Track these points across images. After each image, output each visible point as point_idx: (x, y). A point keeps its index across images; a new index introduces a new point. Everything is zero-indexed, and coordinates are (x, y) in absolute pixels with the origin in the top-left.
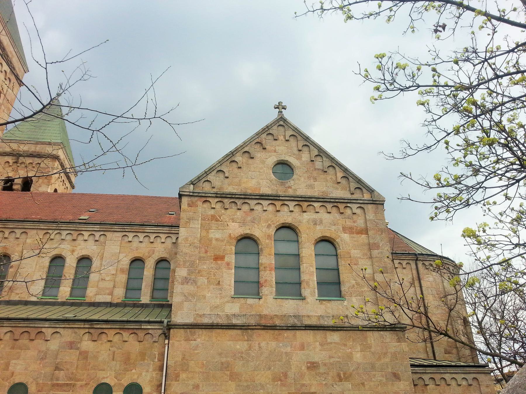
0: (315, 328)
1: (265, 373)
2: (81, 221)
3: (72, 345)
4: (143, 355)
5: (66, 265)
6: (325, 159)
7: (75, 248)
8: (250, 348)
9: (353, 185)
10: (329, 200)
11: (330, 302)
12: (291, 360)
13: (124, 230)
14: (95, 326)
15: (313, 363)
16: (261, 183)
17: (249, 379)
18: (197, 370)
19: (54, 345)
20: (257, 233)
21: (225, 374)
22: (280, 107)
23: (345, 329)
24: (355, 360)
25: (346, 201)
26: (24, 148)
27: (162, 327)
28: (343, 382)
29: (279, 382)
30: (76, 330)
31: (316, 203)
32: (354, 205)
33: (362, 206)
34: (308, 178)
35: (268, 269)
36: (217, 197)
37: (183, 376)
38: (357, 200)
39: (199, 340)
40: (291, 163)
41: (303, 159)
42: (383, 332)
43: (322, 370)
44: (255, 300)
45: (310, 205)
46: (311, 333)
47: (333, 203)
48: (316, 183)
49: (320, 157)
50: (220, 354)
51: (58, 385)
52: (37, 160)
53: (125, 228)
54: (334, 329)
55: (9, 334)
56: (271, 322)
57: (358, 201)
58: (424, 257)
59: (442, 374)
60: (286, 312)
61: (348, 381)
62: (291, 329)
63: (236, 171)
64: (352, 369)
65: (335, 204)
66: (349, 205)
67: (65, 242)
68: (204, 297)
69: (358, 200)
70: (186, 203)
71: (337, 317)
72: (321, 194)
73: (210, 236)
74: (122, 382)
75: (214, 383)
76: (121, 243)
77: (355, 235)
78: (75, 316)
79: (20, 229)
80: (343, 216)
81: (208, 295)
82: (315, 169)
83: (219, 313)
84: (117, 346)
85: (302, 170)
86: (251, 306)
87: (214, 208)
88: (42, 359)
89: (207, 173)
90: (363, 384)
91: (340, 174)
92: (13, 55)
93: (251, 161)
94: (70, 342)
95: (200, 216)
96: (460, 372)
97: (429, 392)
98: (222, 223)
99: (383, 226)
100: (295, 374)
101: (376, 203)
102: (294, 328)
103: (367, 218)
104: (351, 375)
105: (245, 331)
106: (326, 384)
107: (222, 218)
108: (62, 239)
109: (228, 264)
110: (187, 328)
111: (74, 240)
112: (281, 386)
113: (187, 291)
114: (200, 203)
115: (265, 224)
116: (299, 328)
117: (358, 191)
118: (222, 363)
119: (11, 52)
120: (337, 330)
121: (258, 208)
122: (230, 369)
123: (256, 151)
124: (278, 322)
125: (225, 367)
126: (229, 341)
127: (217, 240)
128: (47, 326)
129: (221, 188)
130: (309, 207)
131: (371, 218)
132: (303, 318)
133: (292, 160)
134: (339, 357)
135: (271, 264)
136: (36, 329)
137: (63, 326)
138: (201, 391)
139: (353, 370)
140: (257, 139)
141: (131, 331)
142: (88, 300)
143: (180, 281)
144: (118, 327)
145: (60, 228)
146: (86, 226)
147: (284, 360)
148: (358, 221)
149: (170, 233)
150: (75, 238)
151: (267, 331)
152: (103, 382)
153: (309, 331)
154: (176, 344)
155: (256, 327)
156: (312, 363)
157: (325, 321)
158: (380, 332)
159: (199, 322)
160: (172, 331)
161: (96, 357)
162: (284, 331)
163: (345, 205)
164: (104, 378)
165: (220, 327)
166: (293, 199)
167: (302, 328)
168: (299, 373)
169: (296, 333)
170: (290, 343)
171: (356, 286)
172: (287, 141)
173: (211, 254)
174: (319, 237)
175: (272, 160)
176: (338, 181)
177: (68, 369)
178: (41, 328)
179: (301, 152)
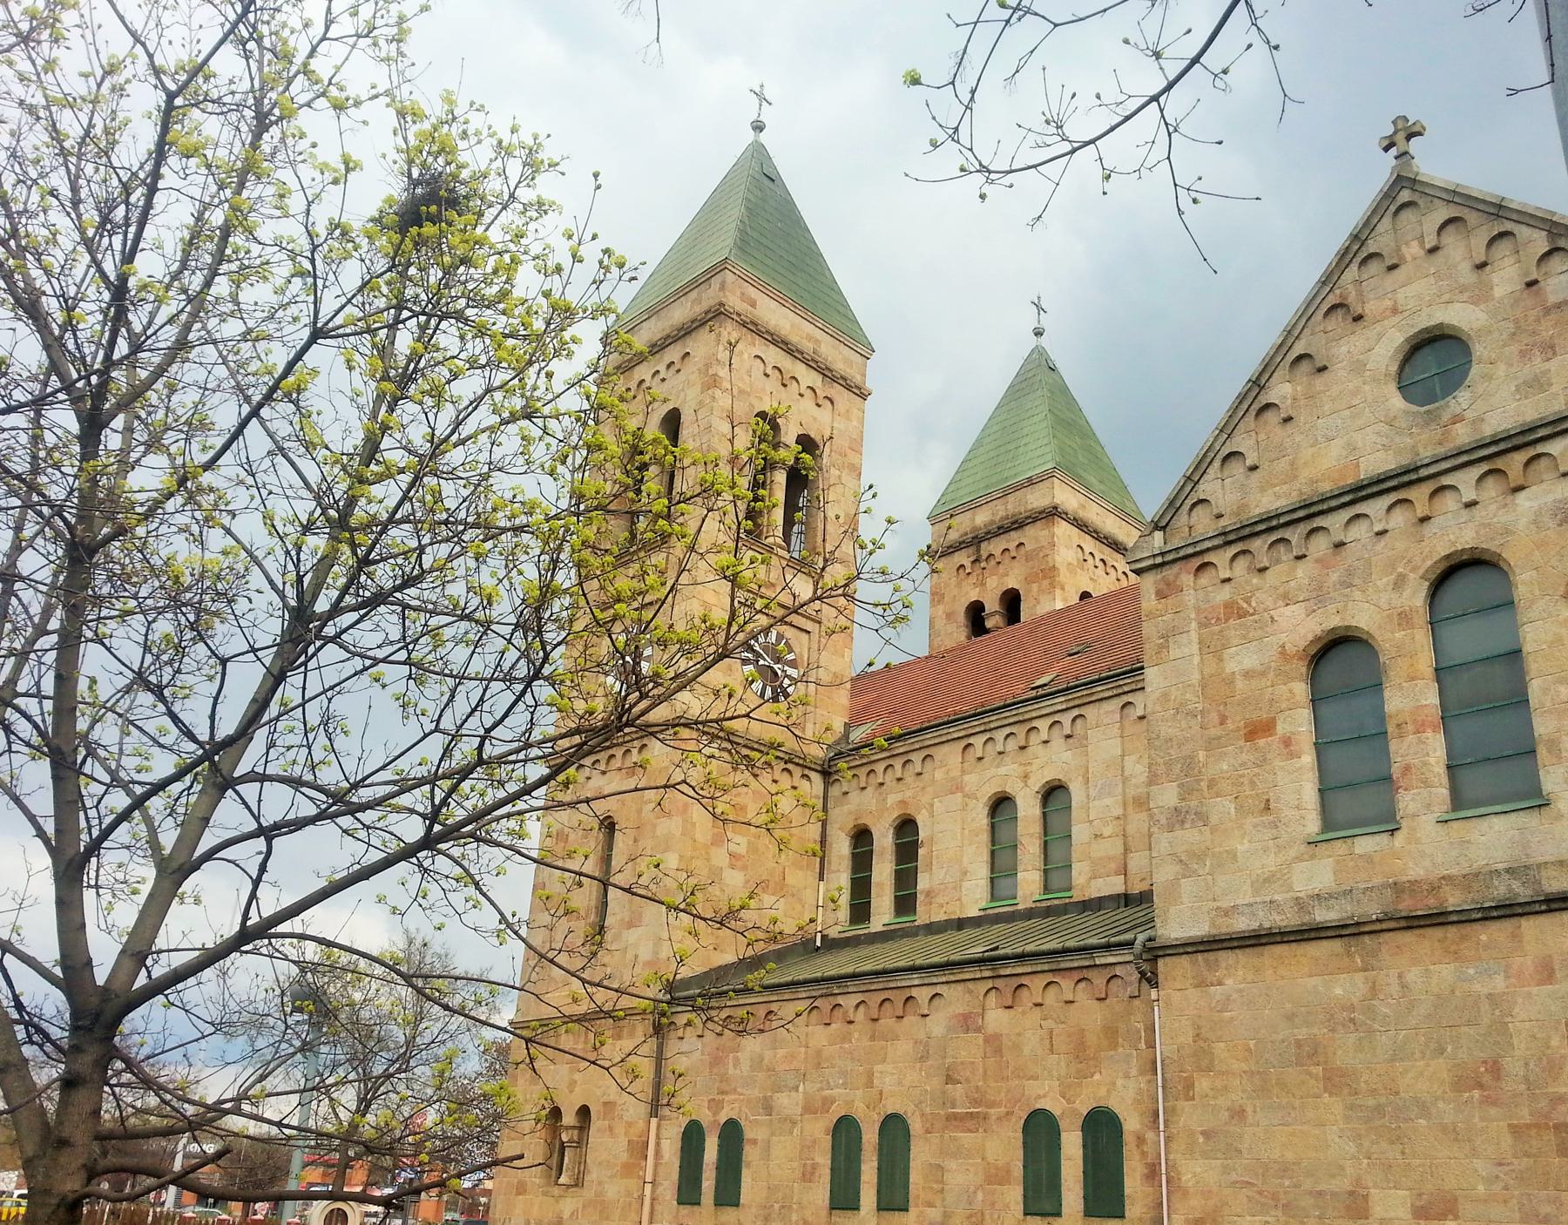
1: (1428, 1065)
2: (1041, 692)
3: (967, 1023)
4: (1111, 1034)
5: (1074, 804)
7: (1029, 768)
8: (1374, 990)
12: (1509, 1019)
13: (1120, 691)
16: (1360, 444)
17: (1379, 1086)
18: (1236, 1066)
19: (938, 1024)
20: (1363, 617)
21: (1310, 1074)
22: (1406, 132)
26: (982, 518)
27: (1131, 958)
29: (1476, 1093)
30: (970, 985)
35: (1410, 727)
37: (1203, 1084)
40: (1454, 327)
41: (1498, 292)
44: (1377, 838)
45: (1538, 456)
48: (1553, 365)
50: (1290, 1017)
51: (955, 1117)
52: (1015, 537)
53: (1121, 683)
55: (862, 1008)
56: (1432, 902)
62: (1499, 917)
63: (1279, 433)
67: (1007, 759)
68: (1234, 856)
70: (1153, 590)
73: (1227, 671)
74: (1077, 1105)
75: (1285, 1101)
76: (1122, 728)
78: (996, 948)
81: (1242, 847)
82: (1547, 311)
83: (1277, 897)
84: (1055, 1016)
85: (1496, 335)
86: (1368, 859)
87: (1229, 580)
88: (923, 1059)
89: (1192, 479)
92: (817, 342)
93: (1320, 382)
94: (963, 1015)
95: (1193, 616)
98: (1256, 617)
100: (1526, 1064)
102: (1508, 910)
105: (1353, 941)
107: (1254, 604)
108: (1000, 753)
109: (1287, 742)
110: (1196, 952)
111: (1023, 748)
112: (1481, 1103)
113: (1185, 847)
114: (1187, 579)
115: (1385, 580)
116: (1527, 909)
118: (1299, 1044)
119: (809, 338)
121: (1360, 531)
122: (1322, 1059)
124: (1454, 900)
125: (1308, 1053)
126: (1311, 976)
127: (1248, 674)
128: (916, 982)
129: (1243, 507)
130: (1535, 466)
132: (1543, 873)
133: (1460, 316)
135: (1418, 708)
137: (944, 979)
138: (1251, 1125)
140: (1331, 296)
141: (1077, 975)
142: (1077, 895)
143: (1163, 821)
144: (1046, 967)
146: (1036, 706)
147: (1486, 1021)
150: (1023, 743)
151: (1422, 931)
152: (1038, 1106)
154: (1176, 997)
155: (1384, 926)
159: (1224, 930)
160: (1161, 962)
161: (1017, 1047)
162: (1477, 926)
164: (1039, 1097)
165: (1278, 939)
166: (1465, 458)
167: (1537, 908)
173: (1236, 722)
179: (1488, 268)
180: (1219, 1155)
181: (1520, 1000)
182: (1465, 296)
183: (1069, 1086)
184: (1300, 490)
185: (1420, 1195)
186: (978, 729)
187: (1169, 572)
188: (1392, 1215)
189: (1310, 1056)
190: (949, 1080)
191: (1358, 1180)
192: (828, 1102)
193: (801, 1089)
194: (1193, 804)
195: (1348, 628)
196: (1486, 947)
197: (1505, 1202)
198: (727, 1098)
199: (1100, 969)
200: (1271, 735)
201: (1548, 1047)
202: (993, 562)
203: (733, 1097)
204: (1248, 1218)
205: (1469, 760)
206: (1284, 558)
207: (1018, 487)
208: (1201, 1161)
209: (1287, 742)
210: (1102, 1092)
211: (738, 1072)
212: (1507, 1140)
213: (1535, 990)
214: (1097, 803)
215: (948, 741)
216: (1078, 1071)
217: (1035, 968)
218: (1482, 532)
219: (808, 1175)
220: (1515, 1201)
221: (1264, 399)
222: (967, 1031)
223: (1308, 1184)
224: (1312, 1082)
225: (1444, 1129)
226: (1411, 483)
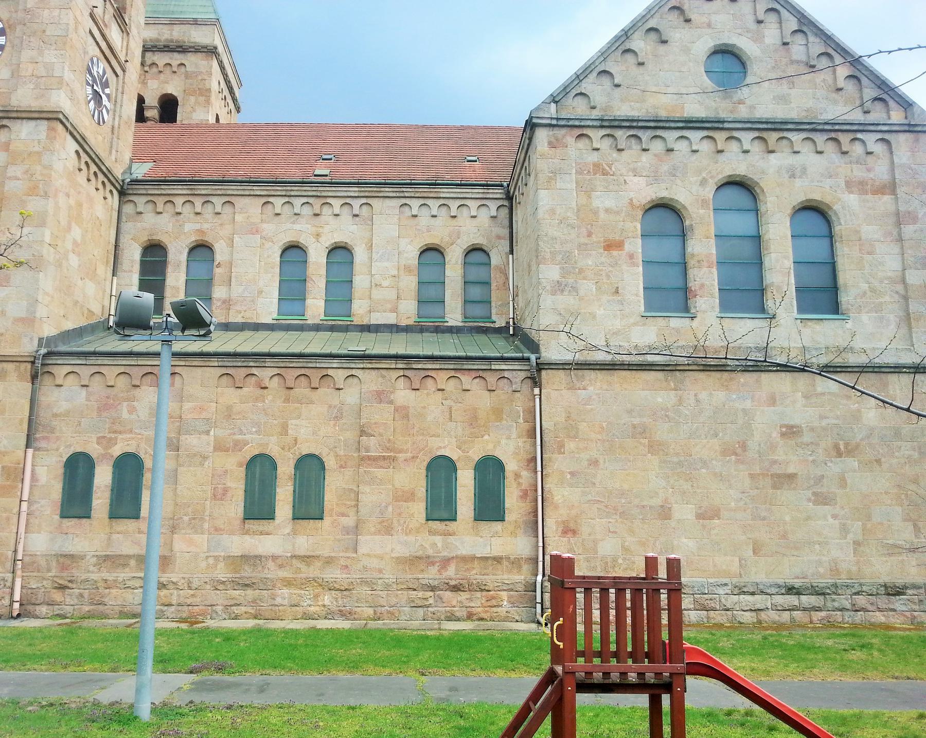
3: (380, 396)
4: (498, 413)
6: (812, 38)
8: (680, 401)
9: (870, 92)
11: (821, 322)
12: (752, 422)
13: (402, 195)
14: (414, 366)
15: (792, 427)
21: (641, 443)
23: (849, 370)
25: (855, 128)
28: (843, 458)
29: (733, 457)
30: (383, 372)
33: (887, 136)
36: (602, 127)
37: (571, 445)
39: (591, 388)
40: (741, 49)
43: (806, 438)
48: (793, 92)
50: (630, 412)
51: (369, 458)
53: (404, 190)
57: (880, 128)
63: (635, 70)
64: (859, 437)
66: (859, 136)
68: (594, 317)
72: (804, 114)
77: (869, 197)
79: (219, 197)
80: (846, 158)
81: (600, 312)
86: (678, 331)
87: (597, 149)
90: (878, 461)
93: (662, 49)
98: (615, 177)
100: (760, 445)
104: (858, 446)
105: (670, 374)
109: (631, 256)
112: (736, 462)
117: (879, 106)
118: (634, 427)
125: (639, 432)
127: (607, 211)
128: (335, 365)
131: (904, 160)
133: (745, 44)
134: (838, 418)
136: (319, 370)
137: (362, 366)
139: (862, 440)
141: (474, 374)
142: (357, 321)
144: (452, 367)
145: (288, 194)
146: (334, 189)
147: (740, 422)
149: (486, 198)
152: (439, 453)
155: (690, 368)
160: (544, 373)
165: (626, 367)
166: (749, 125)
169: (761, 377)
171: (869, 293)
175: (705, 44)
177: (381, 435)
178: (325, 369)
180: (580, 485)
181: (758, 413)
182: (749, 35)
183: (465, 442)
184: (647, 110)
185: (700, 507)
186: (279, 193)
187: (560, 132)
188: (685, 517)
189: (641, 434)
190: (363, 433)
191: (666, 500)
192: (238, 446)
193: (212, 433)
194: (571, 281)
195: (672, 199)
196: (743, 385)
197: (745, 510)
198: (120, 436)
199: (493, 372)
200: (621, 250)
201: (771, 437)
202: (155, 70)
203: (128, 436)
204: (598, 520)
205: (728, 288)
206: (634, 147)
207: (183, 22)
208: (568, 489)
209: (631, 256)
210: (490, 446)
211: (133, 416)
212: (747, 481)
213: (766, 409)
214: (378, 264)
215: (250, 195)
216: (471, 433)
217: (442, 366)
218: (750, 169)
219: (220, 495)
220: (750, 510)
221: (628, 45)
222: (380, 403)
223: (636, 502)
224: (642, 447)
225: (715, 474)
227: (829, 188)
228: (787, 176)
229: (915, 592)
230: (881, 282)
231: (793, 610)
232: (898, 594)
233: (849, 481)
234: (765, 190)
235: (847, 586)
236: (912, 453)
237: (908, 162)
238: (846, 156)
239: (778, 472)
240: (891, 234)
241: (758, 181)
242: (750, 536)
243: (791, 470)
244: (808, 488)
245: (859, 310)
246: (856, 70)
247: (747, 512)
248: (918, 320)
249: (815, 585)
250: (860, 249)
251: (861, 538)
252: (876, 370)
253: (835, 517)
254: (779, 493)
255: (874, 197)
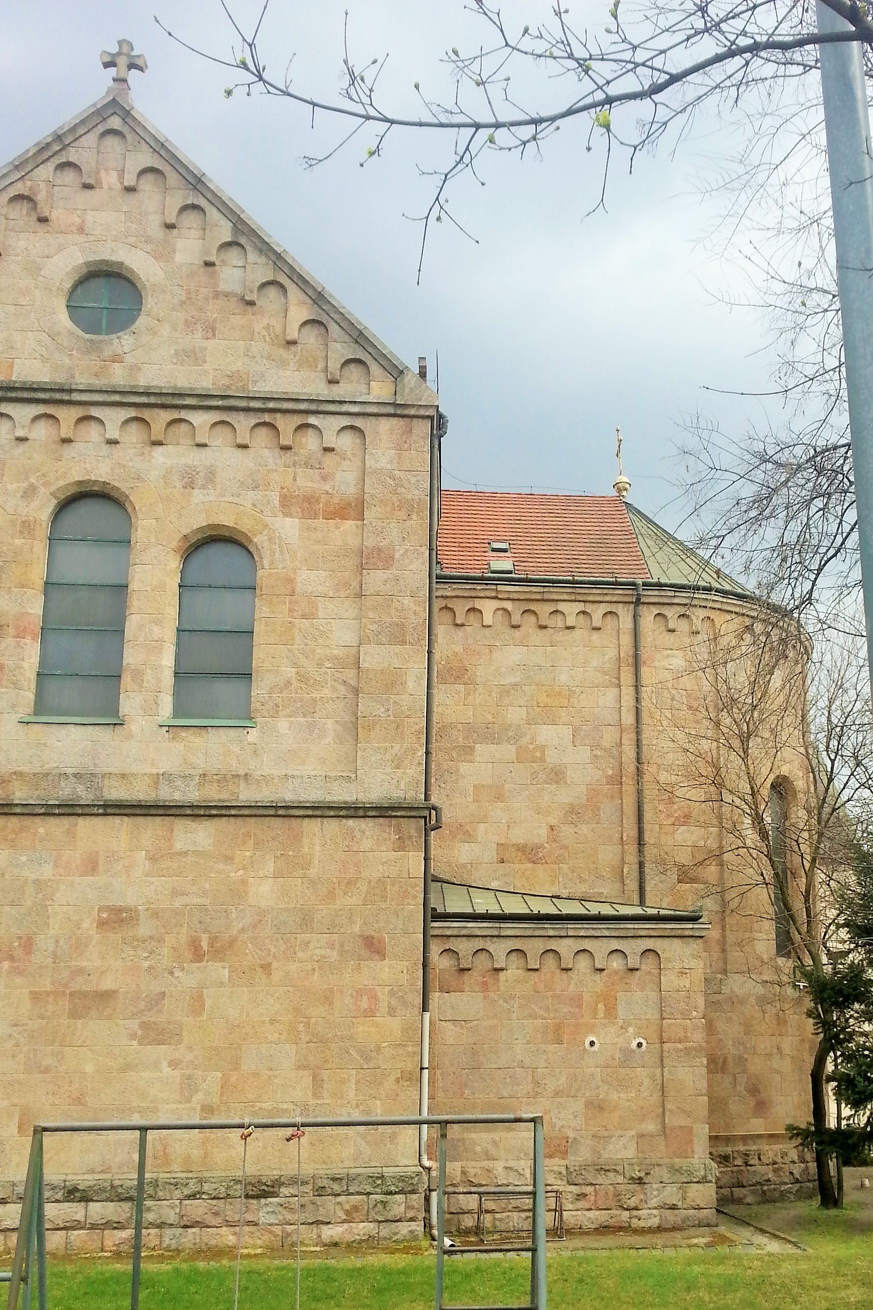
0: (138, 811)
6: (252, 256)
9: (341, 350)
10: (243, 404)
11: (203, 732)
12: (50, 902)
15: (121, 910)
23: (233, 812)
24: (252, 900)
25: (303, 406)
28: (204, 963)
31: (201, 412)
32: (331, 419)
33: (358, 422)
34: (187, 324)
35: (12, 631)
38: (341, 402)
41: (179, 258)
42: (356, 819)
43: (144, 929)
46: (122, 825)
47: (260, 414)
48: (211, 344)
49: (239, 249)
54: (196, 812)
57: (345, 408)
58: (663, 593)
59: (552, 941)
60: (56, 765)
61: (222, 960)
62: (60, 815)
64: (237, 926)
65: (267, 418)
66: (312, 420)
69: (345, 402)
71: (215, 777)
72: (226, 381)
77: (320, 522)
80: (288, 457)
82: (217, 295)
90: (266, 968)
91: (299, 311)
96: (607, 933)
97: (502, 988)
99: (416, 492)
101: (406, 412)
103: (367, 465)
104: (232, 942)
106: (151, 968)
115: (15, 485)
116: (87, 811)
117: (355, 371)
120: (210, 816)
123: (11, 230)
130: (175, 428)
131: (383, 463)
132: (106, 782)
134: (205, 893)
139: (243, 930)
140: (19, 185)
147: (29, 903)
148: (338, 475)
153: (117, 820)
156: (117, 911)
157: (177, 788)
158: (344, 820)
162: (37, 820)
163: (298, 420)
168: (70, 938)
169: (76, 825)
170: (55, 853)
171: (295, 683)
172: (130, 190)
174: (195, 527)
176: (289, 338)
179: (175, 231)
181: (63, 887)
182: (149, 248)
212: (26, 1005)
213: (77, 880)
220: (22, 1055)
226: (61, 402)
227: (250, 506)
228: (179, 485)
229: (293, 1191)
230: (320, 665)
231: (73, 1228)
232: (265, 1195)
233: (208, 1003)
234: (137, 508)
235: (176, 1184)
236: (328, 952)
237: (389, 467)
238: (289, 454)
239: (84, 988)
240: (347, 585)
241: (127, 493)
242: (15, 1100)
243: (107, 984)
244: (133, 1016)
245: (275, 713)
246: (323, 313)
247: (17, 1059)
248: (370, 728)
249: (117, 1183)
250: (290, 610)
251: (216, 1100)
252: (280, 812)
253: (174, 1064)
254: (79, 1026)
255: (327, 524)
